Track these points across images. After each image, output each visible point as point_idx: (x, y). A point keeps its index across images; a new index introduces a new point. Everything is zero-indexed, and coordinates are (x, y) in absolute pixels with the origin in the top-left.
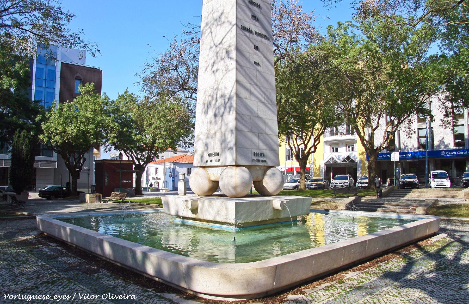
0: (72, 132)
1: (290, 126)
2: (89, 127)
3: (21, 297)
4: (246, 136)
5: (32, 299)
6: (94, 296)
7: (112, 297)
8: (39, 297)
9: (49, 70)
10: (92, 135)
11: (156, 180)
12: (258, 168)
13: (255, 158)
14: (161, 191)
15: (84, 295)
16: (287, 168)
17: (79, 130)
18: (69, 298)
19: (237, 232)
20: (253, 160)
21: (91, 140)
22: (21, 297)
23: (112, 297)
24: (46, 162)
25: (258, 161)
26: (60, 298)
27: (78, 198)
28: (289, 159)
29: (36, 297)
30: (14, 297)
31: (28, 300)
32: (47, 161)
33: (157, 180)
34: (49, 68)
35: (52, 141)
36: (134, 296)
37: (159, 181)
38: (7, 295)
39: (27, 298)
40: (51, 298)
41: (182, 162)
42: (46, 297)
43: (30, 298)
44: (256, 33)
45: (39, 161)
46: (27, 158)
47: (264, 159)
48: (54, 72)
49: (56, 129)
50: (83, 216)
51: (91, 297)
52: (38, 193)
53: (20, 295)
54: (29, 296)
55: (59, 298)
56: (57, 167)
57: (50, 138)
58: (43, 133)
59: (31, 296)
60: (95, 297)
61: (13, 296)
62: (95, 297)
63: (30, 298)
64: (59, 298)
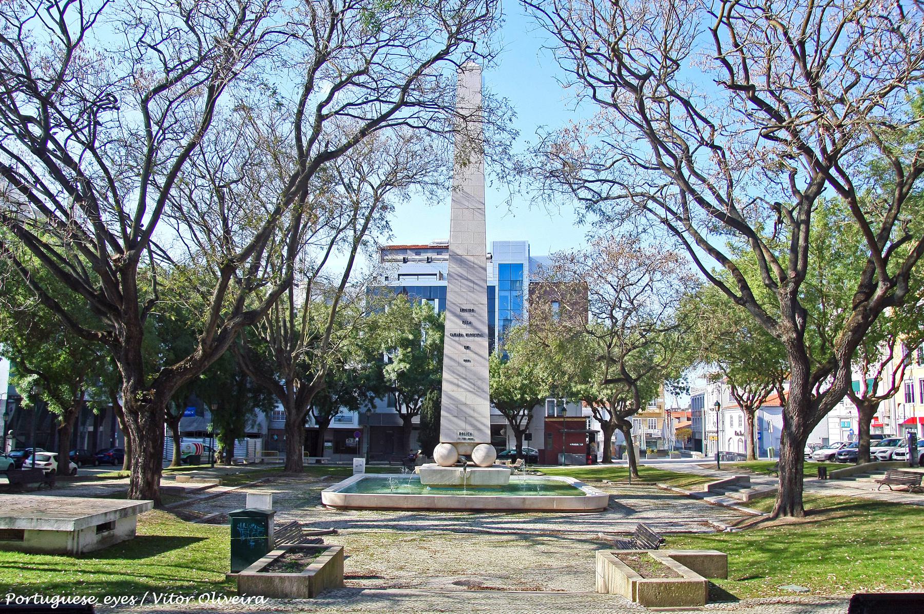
1: (152, 451)
3: (39, 599)
5: (60, 603)
6: (23, 599)
8: (74, 601)
13: (461, 437)
15: (163, 596)
19: (134, 531)
20: (459, 439)
22: (39, 599)
25: (465, 439)
26: (117, 603)
28: (909, 402)
31: (52, 607)
38: (11, 596)
39: (52, 601)
42: (89, 600)
44: (467, 335)
51: (177, 599)
53: (36, 596)
55: (114, 602)
59: (58, 597)
60: (25, 601)
61: (23, 599)
62: (25, 601)
64: (114, 602)
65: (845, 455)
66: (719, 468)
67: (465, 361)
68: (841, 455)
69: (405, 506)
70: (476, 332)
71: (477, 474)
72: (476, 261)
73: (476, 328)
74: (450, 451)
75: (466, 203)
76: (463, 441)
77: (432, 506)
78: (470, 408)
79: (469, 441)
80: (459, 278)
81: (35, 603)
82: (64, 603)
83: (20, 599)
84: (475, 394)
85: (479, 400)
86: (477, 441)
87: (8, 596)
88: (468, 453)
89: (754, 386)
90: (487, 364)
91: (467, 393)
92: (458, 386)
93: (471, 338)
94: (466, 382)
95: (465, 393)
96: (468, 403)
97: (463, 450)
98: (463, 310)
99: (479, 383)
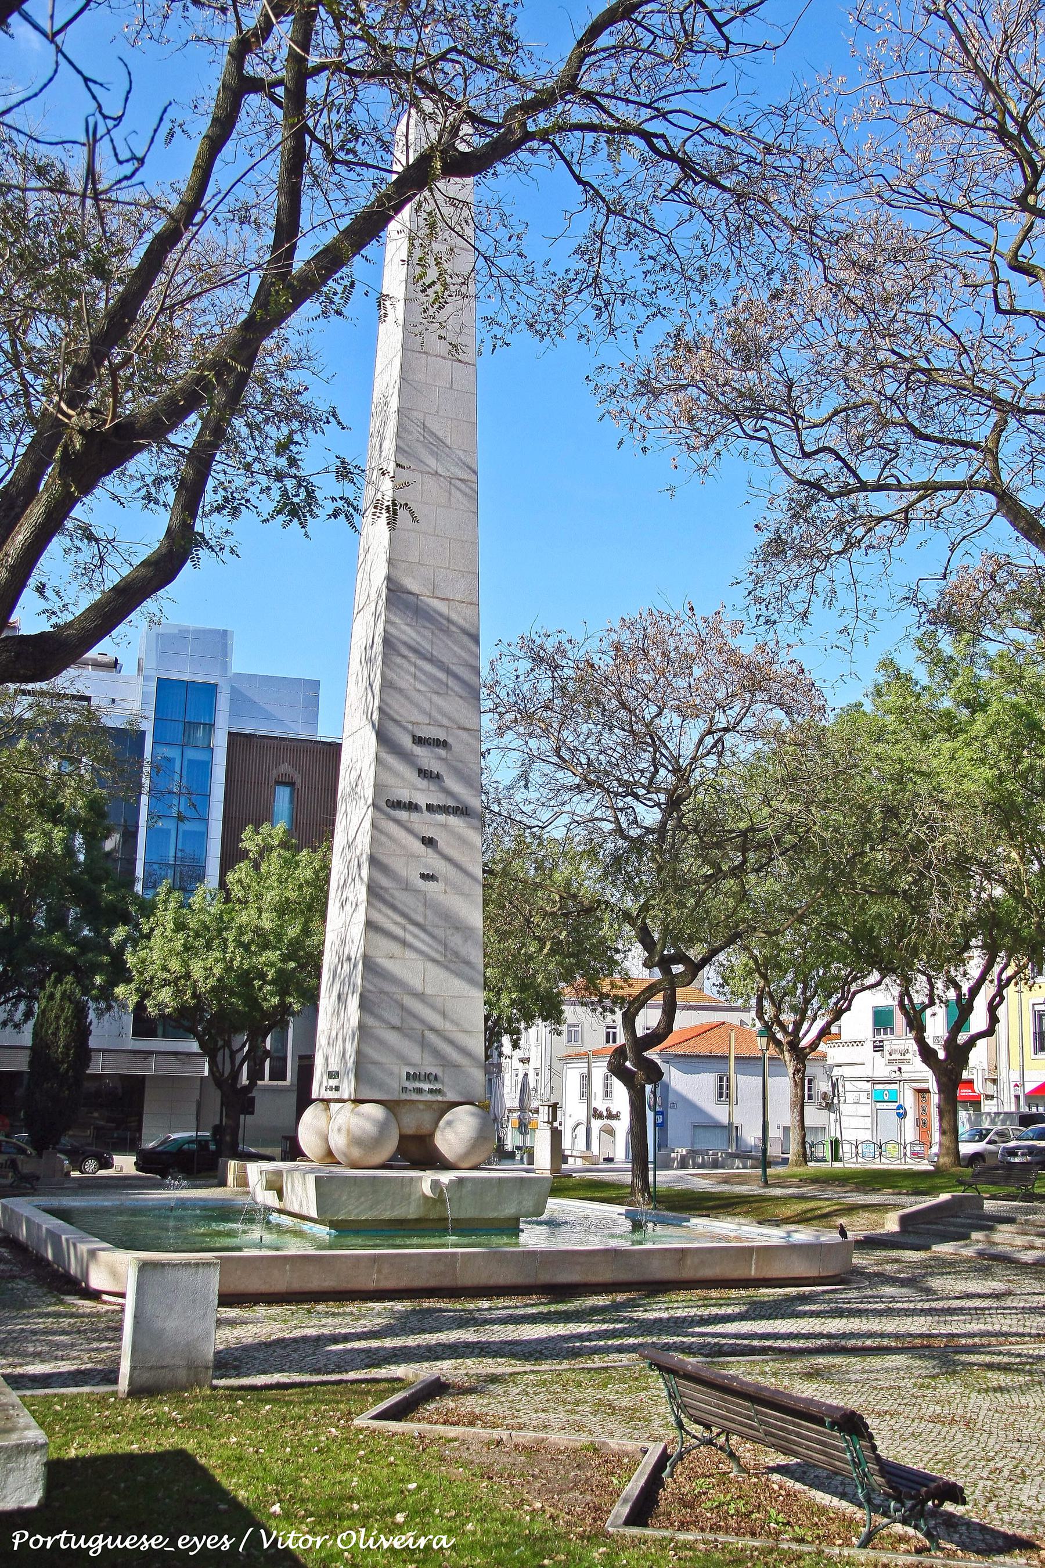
0: (206, 978)
2: (262, 959)
3: (68, 1540)
4: (382, 1043)
5: (105, 1547)
7: (371, 1540)
8: (127, 1543)
9: (191, 762)
10: (270, 983)
11: (605, 1121)
12: (421, 1106)
13: (411, 1085)
14: (571, 1160)
16: (1029, 1087)
17: (229, 969)
18: (228, 1544)
20: (405, 1090)
21: (265, 999)
22: (68, 1540)
23: (371, 1540)
24: (172, 1058)
25: (419, 1091)
26: (199, 1546)
27: (215, 1177)
29: (118, 1541)
30: (45, 1543)
32: (176, 1054)
33: (609, 1122)
34: (191, 754)
35: (148, 1003)
36: (445, 1538)
37: (614, 1123)
38: (22, 1536)
39: (90, 1543)
40: (166, 1546)
41: (696, 1051)
42: (153, 1541)
43: (97, 1545)
44: (430, 808)
45: (151, 1053)
46: (68, 1055)
47: (438, 1086)
48: (205, 768)
49: (165, 968)
50: (106, 1203)
52: (134, 1159)
53: (64, 1534)
54: (96, 1540)
55: (194, 1546)
56: (206, 1074)
57: (145, 995)
58: (129, 980)
59: (101, 1537)
61: (42, 1540)
63: (97, 1545)
64: (194, 1546)
65: (1023, 1155)
66: (766, 1181)
67: (423, 876)
68: (1015, 1155)
69: (372, 1285)
70: (451, 803)
71: (469, 1186)
72: (454, 617)
73: (448, 793)
74: (383, 1127)
75: (432, 462)
76: (415, 1097)
77: (446, 1282)
78: (433, 1007)
79: (429, 1097)
80: (411, 655)
81: (62, 1546)
82: (110, 1547)
83: (36, 1542)
84: (447, 968)
85: (458, 986)
86: (451, 1096)
87: (17, 1534)
88: (426, 1129)
89: (605, 931)
90: (479, 891)
91: (429, 965)
92: (404, 943)
93: (441, 818)
94: (423, 935)
95: (421, 964)
96: (429, 991)
97: (412, 1123)
98: (419, 741)
99: (456, 941)
